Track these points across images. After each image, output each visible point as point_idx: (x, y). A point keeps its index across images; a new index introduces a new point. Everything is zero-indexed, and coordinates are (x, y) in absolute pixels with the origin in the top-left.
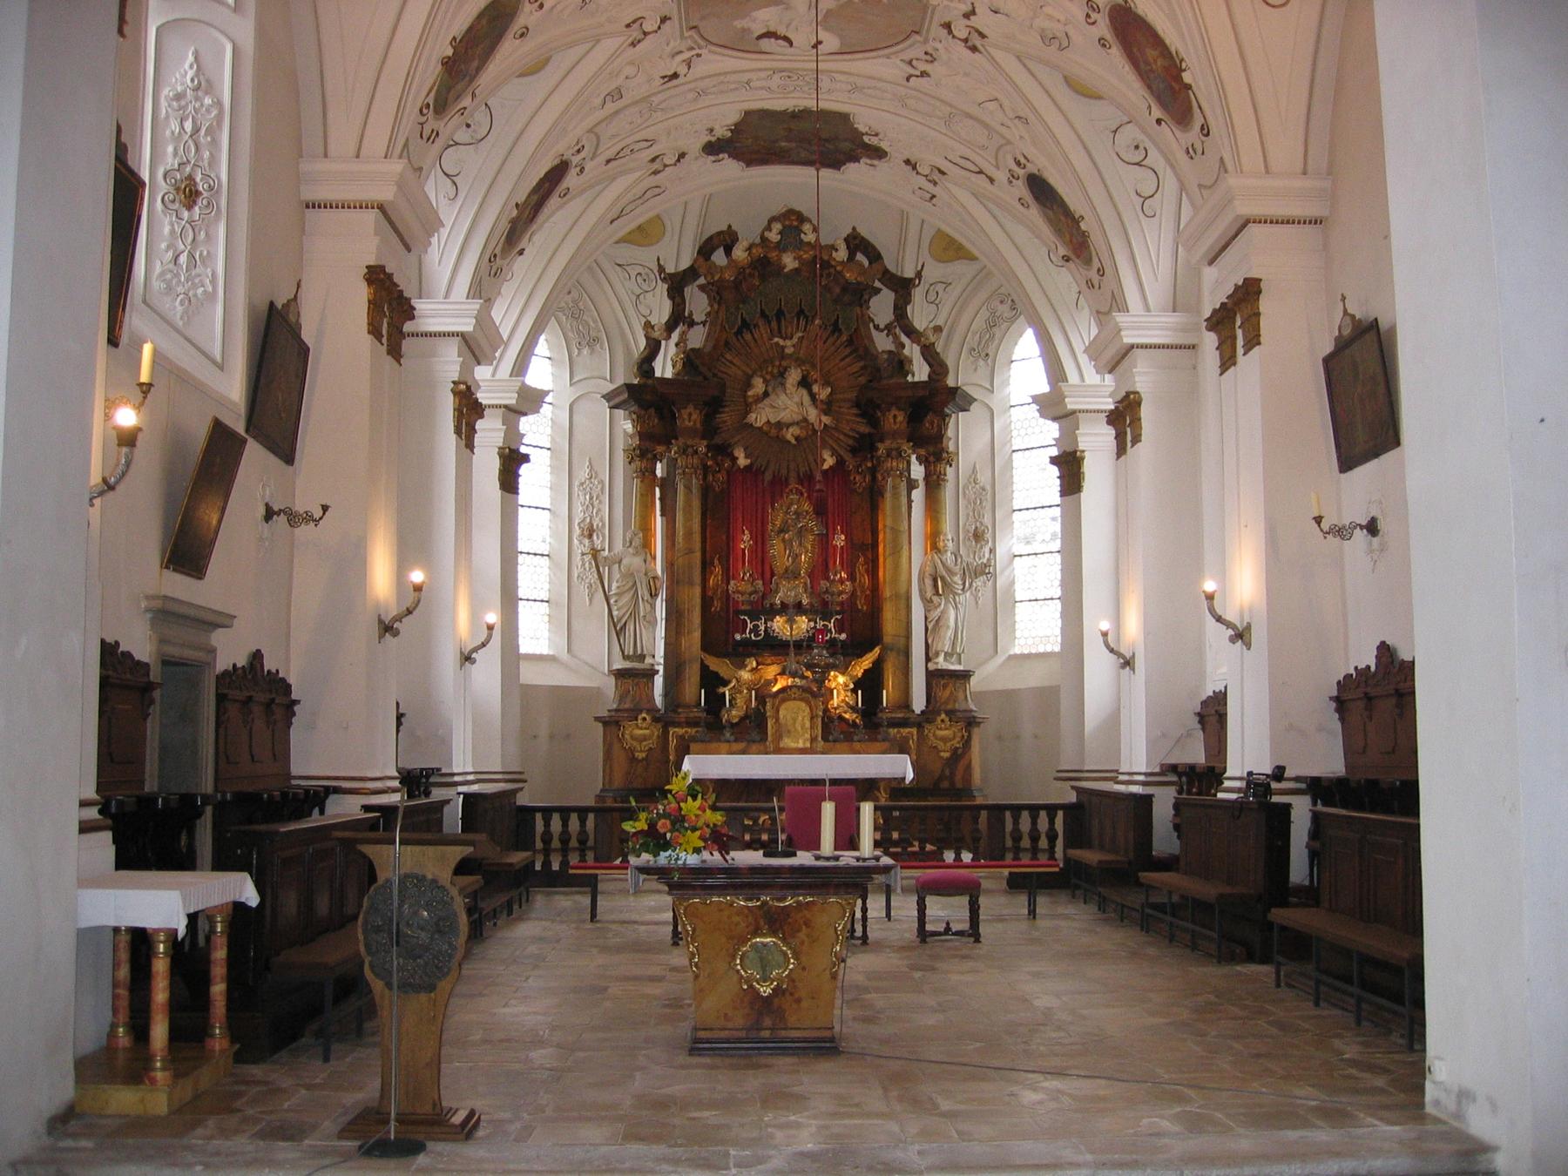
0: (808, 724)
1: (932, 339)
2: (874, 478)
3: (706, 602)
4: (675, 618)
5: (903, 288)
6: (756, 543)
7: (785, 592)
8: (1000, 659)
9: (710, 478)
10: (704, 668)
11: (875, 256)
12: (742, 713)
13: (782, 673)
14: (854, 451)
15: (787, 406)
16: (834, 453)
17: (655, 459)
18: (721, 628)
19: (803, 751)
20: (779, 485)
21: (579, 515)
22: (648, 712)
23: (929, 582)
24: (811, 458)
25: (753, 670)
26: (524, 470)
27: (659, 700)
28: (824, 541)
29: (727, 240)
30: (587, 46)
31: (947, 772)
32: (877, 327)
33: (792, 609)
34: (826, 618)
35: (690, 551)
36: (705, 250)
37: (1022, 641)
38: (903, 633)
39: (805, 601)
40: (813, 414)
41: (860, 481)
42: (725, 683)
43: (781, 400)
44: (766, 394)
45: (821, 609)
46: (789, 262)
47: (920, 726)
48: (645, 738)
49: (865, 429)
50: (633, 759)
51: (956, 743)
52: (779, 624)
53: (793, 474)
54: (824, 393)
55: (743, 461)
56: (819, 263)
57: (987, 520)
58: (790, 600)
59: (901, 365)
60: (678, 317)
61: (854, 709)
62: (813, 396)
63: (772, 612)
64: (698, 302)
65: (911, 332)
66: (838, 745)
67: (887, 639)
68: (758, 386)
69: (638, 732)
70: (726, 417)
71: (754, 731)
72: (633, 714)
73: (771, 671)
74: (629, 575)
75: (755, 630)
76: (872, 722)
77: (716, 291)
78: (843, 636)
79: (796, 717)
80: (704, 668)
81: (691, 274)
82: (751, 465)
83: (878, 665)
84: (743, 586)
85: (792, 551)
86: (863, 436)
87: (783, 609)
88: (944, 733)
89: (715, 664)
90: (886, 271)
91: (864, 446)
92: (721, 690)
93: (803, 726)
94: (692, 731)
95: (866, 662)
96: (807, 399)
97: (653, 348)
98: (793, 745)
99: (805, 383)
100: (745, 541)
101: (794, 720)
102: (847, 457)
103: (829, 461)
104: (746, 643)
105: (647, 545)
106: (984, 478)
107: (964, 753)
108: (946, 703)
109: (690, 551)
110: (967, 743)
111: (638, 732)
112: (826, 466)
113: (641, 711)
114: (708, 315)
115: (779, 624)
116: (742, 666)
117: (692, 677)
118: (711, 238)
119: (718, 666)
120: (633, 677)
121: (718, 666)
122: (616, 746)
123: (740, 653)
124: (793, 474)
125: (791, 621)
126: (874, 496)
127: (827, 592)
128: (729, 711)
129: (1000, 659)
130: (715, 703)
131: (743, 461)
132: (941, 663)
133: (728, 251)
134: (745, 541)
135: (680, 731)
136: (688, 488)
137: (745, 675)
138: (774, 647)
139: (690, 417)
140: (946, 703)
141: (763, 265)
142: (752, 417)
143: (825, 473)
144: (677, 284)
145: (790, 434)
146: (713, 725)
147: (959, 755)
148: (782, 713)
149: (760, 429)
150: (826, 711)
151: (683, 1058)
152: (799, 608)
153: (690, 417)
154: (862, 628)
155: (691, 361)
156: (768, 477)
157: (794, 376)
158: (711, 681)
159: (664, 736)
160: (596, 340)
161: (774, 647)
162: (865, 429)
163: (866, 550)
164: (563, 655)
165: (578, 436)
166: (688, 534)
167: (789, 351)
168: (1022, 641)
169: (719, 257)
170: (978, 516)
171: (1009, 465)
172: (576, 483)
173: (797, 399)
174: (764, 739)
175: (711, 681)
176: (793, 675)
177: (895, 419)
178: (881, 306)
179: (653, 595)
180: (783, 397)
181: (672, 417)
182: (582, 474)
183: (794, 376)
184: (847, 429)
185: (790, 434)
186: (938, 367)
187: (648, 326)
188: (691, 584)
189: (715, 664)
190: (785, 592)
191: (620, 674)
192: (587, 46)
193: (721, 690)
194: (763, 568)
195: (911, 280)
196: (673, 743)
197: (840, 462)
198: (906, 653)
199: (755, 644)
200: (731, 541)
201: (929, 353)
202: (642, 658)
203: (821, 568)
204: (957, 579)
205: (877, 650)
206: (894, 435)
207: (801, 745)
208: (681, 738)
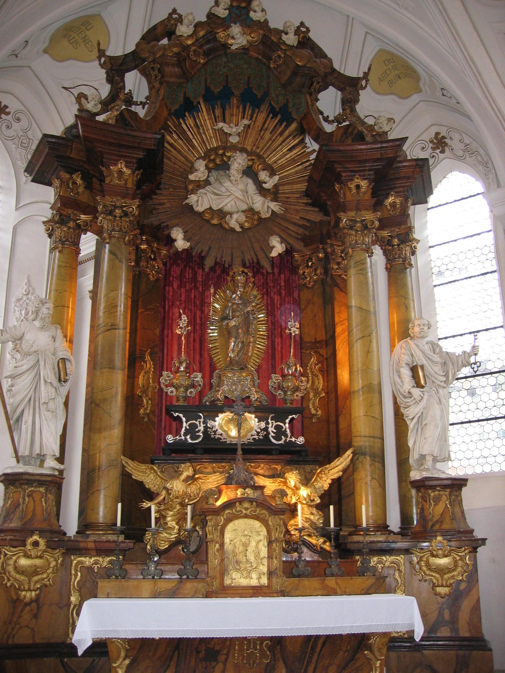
0: (264, 552)
1: (386, 129)
2: (326, 271)
3: (132, 402)
6: (194, 330)
7: (231, 385)
9: (143, 263)
10: (126, 476)
12: (173, 537)
13: (229, 481)
14: (307, 241)
15: (231, 195)
17: (82, 229)
19: (256, 592)
20: (221, 275)
22: (42, 532)
24: (257, 246)
25: (188, 478)
28: (276, 330)
30: (177, 652)
31: (447, 615)
32: (326, 119)
33: (236, 405)
34: (280, 416)
35: (113, 327)
37: (456, 464)
38: (378, 434)
39: (254, 396)
41: (310, 275)
42: (151, 496)
44: (207, 182)
45: (266, 410)
48: (35, 571)
51: (458, 575)
53: (237, 261)
55: (181, 244)
58: (235, 395)
61: (324, 533)
62: (259, 184)
63: (213, 410)
66: (306, 582)
67: (358, 442)
69: (23, 562)
70: (164, 199)
71: (193, 564)
73: (212, 480)
75: (192, 431)
78: (301, 440)
79: (246, 542)
82: (191, 248)
83: (350, 470)
84: (178, 381)
87: (228, 404)
92: (146, 505)
93: (257, 554)
94: (105, 561)
95: (336, 469)
96: (251, 187)
98: (244, 582)
99: (249, 172)
101: (246, 545)
102: (298, 245)
107: (468, 590)
108: (440, 521)
110: (473, 574)
111: (23, 562)
112: (274, 254)
113: (32, 533)
114: (147, 98)
116: (177, 474)
118: (155, 27)
119: (148, 476)
121: (148, 476)
124: (237, 261)
126: (331, 287)
127: (279, 387)
128: (157, 533)
131: (181, 244)
135: (88, 561)
137: (177, 486)
138: (215, 450)
140: (440, 521)
142: (193, 199)
148: (228, 536)
149: (200, 215)
150: (398, 534)
152: (247, 404)
154: (318, 435)
156: (209, 263)
157: (239, 161)
158: (134, 494)
159: (66, 566)
161: (215, 450)
163: (322, 348)
167: (234, 140)
168: (456, 464)
171: (432, 296)
172: (13, 300)
173: (241, 186)
175: (134, 494)
176: (244, 484)
180: (227, 184)
182: (19, 291)
183: (239, 161)
184: (296, 218)
188: (111, 367)
190: (231, 385)
192: (177, 652)
193: (146, 505)
195: (358, 79)
197: (289, 252)
198: (379, 458)
200: (166, 323)
203: (272, 360)
204: (438, 369)
207: (254, 582)
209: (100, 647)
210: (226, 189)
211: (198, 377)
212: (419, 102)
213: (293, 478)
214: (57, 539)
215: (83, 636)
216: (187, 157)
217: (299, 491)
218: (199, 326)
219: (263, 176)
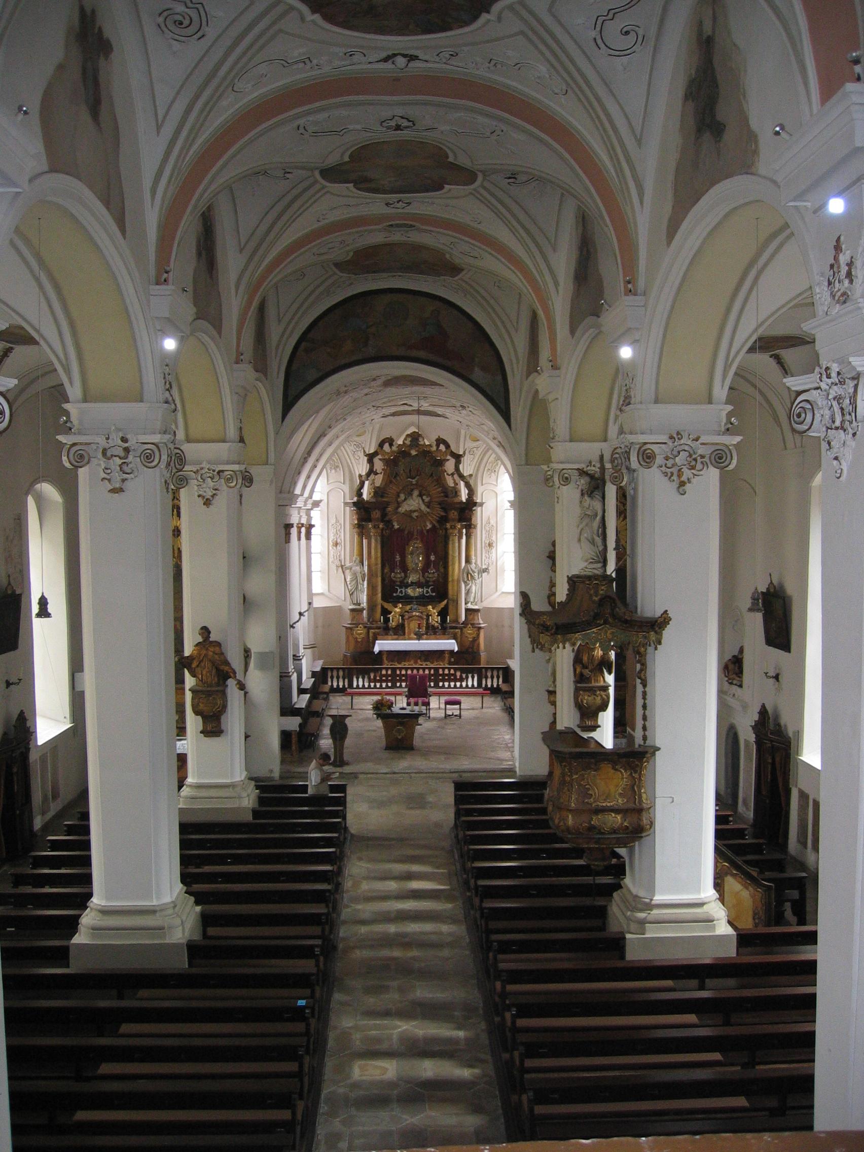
3: (383, 580)
4: (372, 587)
5: (458, 458)
8: (498, 593)
11: (448, 446)
15: (414, 504)
16: (431, 523)
18: (389, 589)
21: (332, 537)
23: (465, 575)
26: (313, 530)
27: (365, 620)
28: (427, 557)
29: (391, 441)
36: (381, 445)
40: (423, 507)
42: (390, 613)
43: (410, 502)
44: (405, 499)
46: (414, 453)
47: (461, 629)
49: (443, 514)
50: (357, 642)
52: (410, 591)
54: (427, 499)
55: (396, 527)
56: (426, 453)
57: (494, 538)
59: (456, 493)
60: (371, 472)
62: (423, 500)
64: (379, 465)
65: (462, 477)
67: (450, 596)
68: (402, 496)
71: (399, 632)
72: (357, 625)
74: (355, 575)
75: (401, 592)
76: (442, 630)
77: (387, 462)
80: (382, 607)
81: (375, 454)
83: (446, 607)
84: (398, 575)
85: (416, 560)
86: (442, 516)
88: (469, 631)
89: (386, 606)
90: (452, 452)
91: (443, 520)
96: (421, 502)
97: (362, 484)
99: (421, 495)
100: (398, 558)
103: (429, 526)
104: (399, 598)
105: (362, 562)
106: (493, 522)
109: (376, 564)
110: (478, 635)
115: (410, 591)
117: (379, 610)
119: (388, 606)
120: (356, 612)
121: (388, 606)
122: (351, 638)
123: (395, 601)
125: (414, 589)
129: (498, 593)
130: (387, 620)
131: (396, 527)
132: (470, 606)
133: (391, 445)
134: (398, 558)
136: (376, 541)
137: (398, 610)
139: (376, 514)
141: (403, 453)
143: (428, 531)
144: (371, 458)
145: (415, 515)
146: (387, 631)
147: (476, 639)
151: (729, 136)
153: (376, 514)
155: (378, 492)
157: (416, 493)
158: (385, 612)
160: (337, 467)
162: (443, 514)
164: (327, 593)
165: (330, 505)
166: (376, 558)
169: (386, 447)
170: (489, 536)
174: (404, 634)
177: (454, 514)
178: (450, 465)
179: (363, 581)
181: (367, 513)
182: (333, 521)
183: (416, 493)
185: (415, 515)
186: (471, 492)
187: (360, 476)
189: (386, 606)
191: (352, 610)
194: (405, 569)
196: (371, 635)
197: (434, 526)
199: (401, 598)
201: (468, 485)
202: (359, 604)
203: (425, 570)
205: (446, 601)
206: (453, 520)
208: (374, 633)
209: (380, 652)
210: (405, 56)
211: (403, 574)
212: (516, 34)
213: (430, 607)
214: (359, 127)
215: (377, 649)
216: (404, 935)
217: (433, 611)
218: (403, 557)
219: (424, 497)
